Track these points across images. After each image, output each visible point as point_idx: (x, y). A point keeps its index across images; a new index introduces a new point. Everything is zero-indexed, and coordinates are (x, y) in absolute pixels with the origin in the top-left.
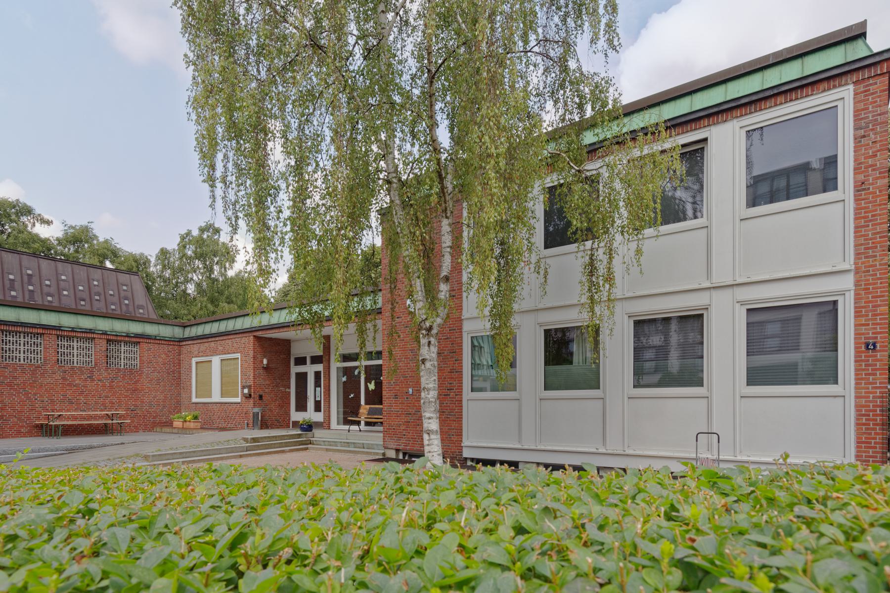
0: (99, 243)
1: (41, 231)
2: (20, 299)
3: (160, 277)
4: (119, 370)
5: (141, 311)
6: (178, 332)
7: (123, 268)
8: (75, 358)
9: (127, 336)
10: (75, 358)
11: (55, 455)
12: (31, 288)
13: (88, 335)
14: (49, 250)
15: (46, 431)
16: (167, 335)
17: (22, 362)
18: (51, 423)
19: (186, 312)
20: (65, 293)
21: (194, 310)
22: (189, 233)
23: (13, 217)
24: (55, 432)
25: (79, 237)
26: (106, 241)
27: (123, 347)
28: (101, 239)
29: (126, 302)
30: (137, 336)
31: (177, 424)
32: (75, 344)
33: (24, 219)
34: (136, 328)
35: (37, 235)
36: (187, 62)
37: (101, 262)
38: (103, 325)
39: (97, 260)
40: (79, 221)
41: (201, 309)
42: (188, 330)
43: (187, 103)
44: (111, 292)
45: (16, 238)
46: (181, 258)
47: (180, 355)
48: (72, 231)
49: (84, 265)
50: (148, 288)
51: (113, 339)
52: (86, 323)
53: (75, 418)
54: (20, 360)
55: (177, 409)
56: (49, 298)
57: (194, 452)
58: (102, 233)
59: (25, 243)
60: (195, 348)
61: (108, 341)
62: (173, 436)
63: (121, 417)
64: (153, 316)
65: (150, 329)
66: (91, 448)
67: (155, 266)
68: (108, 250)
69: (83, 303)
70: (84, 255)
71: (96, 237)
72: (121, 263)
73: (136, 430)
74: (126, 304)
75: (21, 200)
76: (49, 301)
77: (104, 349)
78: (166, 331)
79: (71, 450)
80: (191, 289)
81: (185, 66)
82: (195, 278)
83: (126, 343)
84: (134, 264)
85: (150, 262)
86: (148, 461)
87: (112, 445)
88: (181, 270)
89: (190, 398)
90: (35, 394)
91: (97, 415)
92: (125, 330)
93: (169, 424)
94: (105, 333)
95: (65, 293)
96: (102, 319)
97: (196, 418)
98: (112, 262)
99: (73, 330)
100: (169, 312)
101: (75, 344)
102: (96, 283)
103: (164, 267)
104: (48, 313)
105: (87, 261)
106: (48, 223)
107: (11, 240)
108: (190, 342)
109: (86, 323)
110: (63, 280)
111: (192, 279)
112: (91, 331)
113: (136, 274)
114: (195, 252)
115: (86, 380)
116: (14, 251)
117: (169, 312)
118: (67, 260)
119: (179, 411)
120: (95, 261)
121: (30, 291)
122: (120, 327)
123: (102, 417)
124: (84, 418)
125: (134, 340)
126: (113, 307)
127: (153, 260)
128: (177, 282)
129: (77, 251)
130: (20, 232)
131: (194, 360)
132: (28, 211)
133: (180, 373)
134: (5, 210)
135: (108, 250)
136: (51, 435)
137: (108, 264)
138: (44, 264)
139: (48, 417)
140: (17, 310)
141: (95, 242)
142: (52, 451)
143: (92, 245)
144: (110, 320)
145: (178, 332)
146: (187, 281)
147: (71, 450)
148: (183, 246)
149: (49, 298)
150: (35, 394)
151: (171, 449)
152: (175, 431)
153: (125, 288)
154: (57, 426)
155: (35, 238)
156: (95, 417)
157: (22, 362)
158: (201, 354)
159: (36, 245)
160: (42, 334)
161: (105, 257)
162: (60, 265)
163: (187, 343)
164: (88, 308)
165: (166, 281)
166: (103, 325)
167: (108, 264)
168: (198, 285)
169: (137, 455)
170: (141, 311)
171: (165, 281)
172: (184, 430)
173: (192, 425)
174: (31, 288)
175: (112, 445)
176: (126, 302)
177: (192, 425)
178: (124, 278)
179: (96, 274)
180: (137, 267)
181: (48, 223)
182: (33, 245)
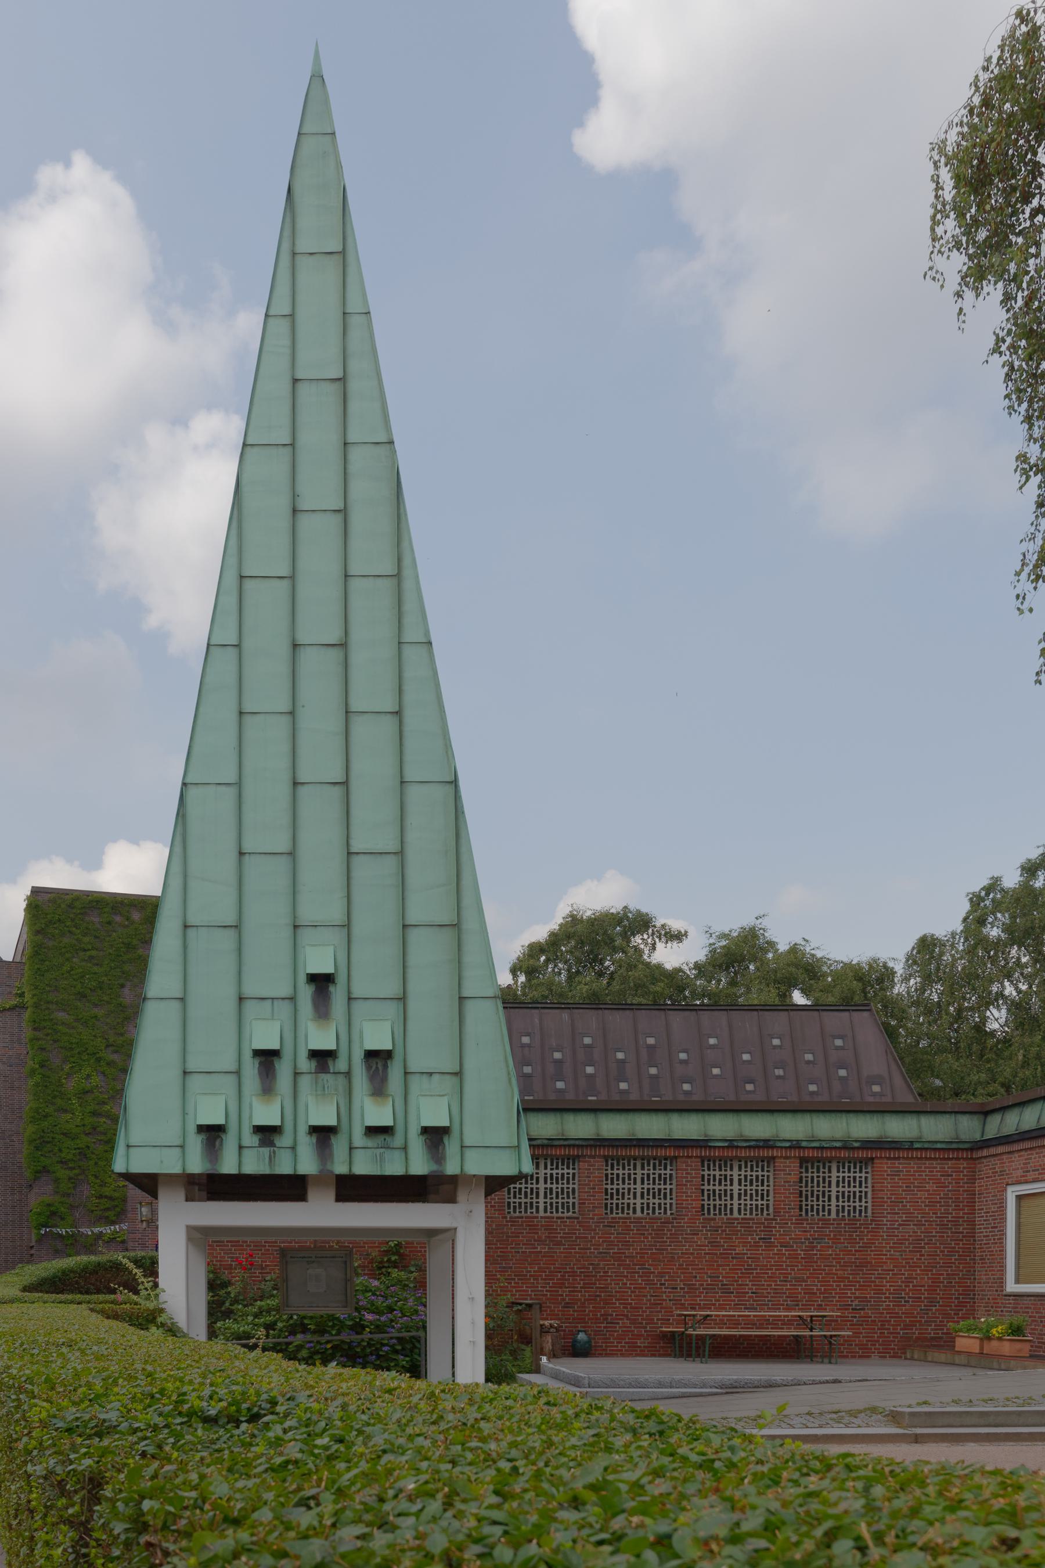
0: (778, 956)
1: (668, 956)
2: (634, 1096)
3: (916, 1003)
4: (826, 1222)
5: (876, 1088)
6: (968, 1128)
7: (831, 999)
8: (736, 1202)
9: (844, 1148)
10: (736, 1202)
11: (701, 1395)
12: (653, 1071)
13: (762, 1152)
14: (681, 989)
15: (681, 1347)
16: (940, 1137)
17: (639, 1213)
18: (690, 1331)
19: (983, 1076)
20: (716, 1071)
21: (1006, 1070)
22: (994, 885)
23: (618, 942)
24: (698, 1348)
25: (739, 953)
26: (794, 949)
27: (834, 1173)
28: (783, 947)
29: (842, 1073)
30: (868, 1145)
31: (966, 1343)
32: (735, 1172)
33: (637, 940)
34: (864, 1128)
35: (659, 967)
36: (1025, 472)
37: (785, 995)
38: (791, 1128)
39: (774, 992)
40: (733, 921)
41: (1025, 1064)
42: (994, 1121)
43: (1018, 574)
44: (809, 1057)
45: (624, 980)
46: (971, 951)
47: (972, 1180)
48: (724, 943)
49: (751, 1008)
50: (891, 1034)
51: (812, 1157)
52: (757, 1127)
53: (734, 1323)
54: (635, 1211)
55: (965, 1305)
56: (686, 1087)
57: (1019, 1414)
58: (783, 937)
59: (639, 987)
60: (1016, 1161)
61: (803, 1161)
62: (957, 1372)
63: (829, 1323)
64: (906, 1097)
65: (898, 1128)
66: (770, 1385)
67: (906, 979)
68: (797, 966)
69: (749, 1087)
70: (749, 990)
71: (771, 944)
72: (827, 990)
73: (861, 1352)
74: (841, 1078)
75: (632, 907)
76: (686, 1093)
77: (794, 1178)
78: (935, 1129)
79: (732, 1389)
80: (997, 1019)
81: (1017, 478)
82: (1009, 990)
83: (841, 1162)
84: (856, 985)
85: (893, 973)
86: (899, 1425)
87: (814, 1383)
88: (971, 977)
89: (1001, 1282)
90: (661, 1274)
91: (780, 1319)
92: (839, 1135)
93: (944, 1343)
94: (796, 1145)
95: (716, 1071)
96: (789, 1116)
97: (1017, 1330)
98: (805, 992)
99: (731, 1144)
100: (938, 1083)
101: (735, 1172)
102: (776, 1042)
103: (928, 979)
104: (686, 1115)
105: (754, 999)
106: (678, 937)
107: (616, 986)
108: (1000, 1149)
109: (757, 1127)
110: (713, 1047)
111: (1001, 995)
112: (766, 1144)
113: (864, 1007)
114: (1007, 929)
115: (756, 1245)
116: (622, 1006)
117: (938, 1083)
118: (719, 1004)
119: (971, 1314)
120: (771, 996)
121: (652, 1077)
122: (827, 1128)
123: (788, 1323)
124: (750, 1323)
125: (861, 1154)
126: (813, 1088)
127: (899, 968)
128: (960, 1011)
129: (733, 983)
130: (631, 967)
131: (1011, 1194)
132: (642, 923)
133: (972, 1223)
134: (605, 933)
135: (797, 966)
136: (689, 1355)
137: (798, 998)
138: (677, 1019)
139: (684, 1320)
140: (631, 1117)
141: (770, 955)
142: (695, 1386)
143: (763, 962)
144: (807, 1117)
145: (968, 1128)
146: (988, 1001)
147: (732, 1389)
148: (976, 919)
149: (686, 1087)
150: (661, 1274)
151: (956, 1402)
152: (962, 1359)
153: (839, 1042)
154: (701, 1338)
155: (658, 972)
156: (775, 1323)
157: (639, 1213)
158: (1031, 1176)
159: (659, 987)
160: (575, 1158)
161: (791, 983)
162: (705, 1016)
163: (993, 1151)
164: (760, 1097)
165: (930, 1010)
166: (791, 1128)
167: (798, 998)
168: (1017, 1007)
169: (873, 1410)
170: (876, 1088)
171: (928, 1012)
172: (984, 1360)
173: (1006, 1348)
174: (653, 1071)
175: (814, 1383)
176: (842, 1073)
177: (1006, 1348)
178: (835, 1021)
179: (779, 1021)
180: (864, 991)
181: (678, 937)
182: (652, 988)
